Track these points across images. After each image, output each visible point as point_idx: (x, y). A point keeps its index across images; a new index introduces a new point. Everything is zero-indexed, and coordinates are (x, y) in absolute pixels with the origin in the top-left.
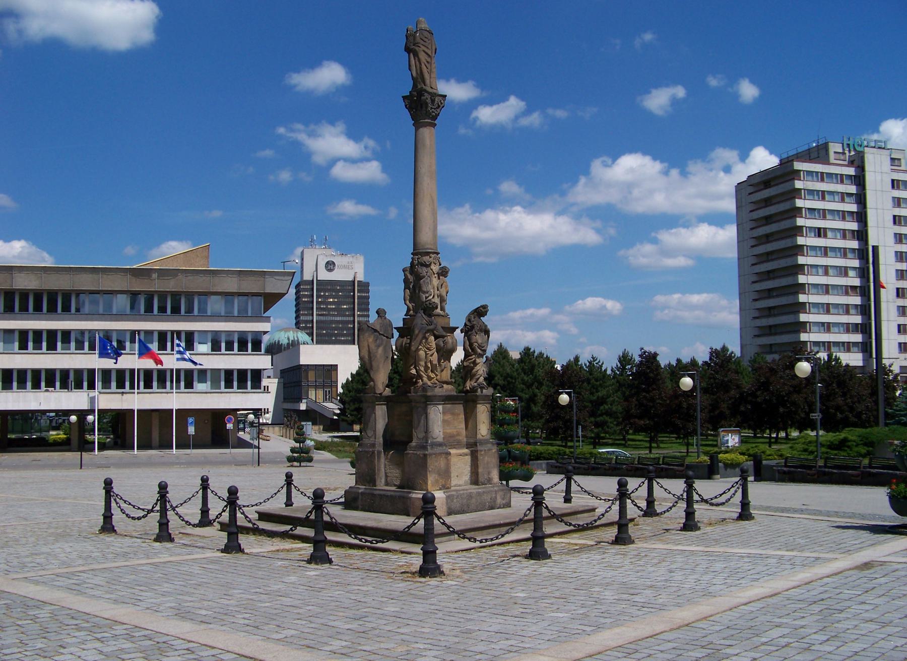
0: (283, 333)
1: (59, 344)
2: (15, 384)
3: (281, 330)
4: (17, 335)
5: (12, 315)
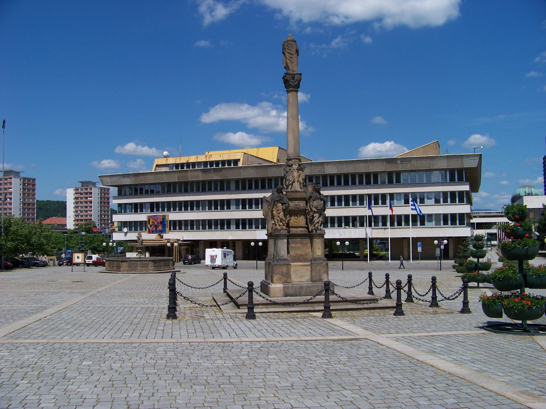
0: (522, 189)
1: (351, 203)
2: (329, 225)
3: (521, 187)
4: (403, 196)
5: (326, 188)
